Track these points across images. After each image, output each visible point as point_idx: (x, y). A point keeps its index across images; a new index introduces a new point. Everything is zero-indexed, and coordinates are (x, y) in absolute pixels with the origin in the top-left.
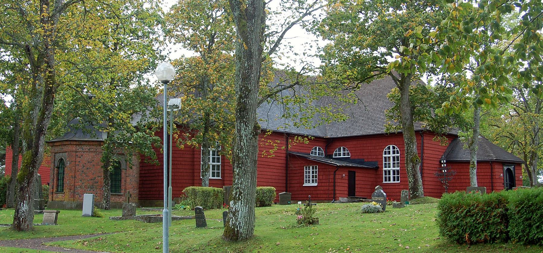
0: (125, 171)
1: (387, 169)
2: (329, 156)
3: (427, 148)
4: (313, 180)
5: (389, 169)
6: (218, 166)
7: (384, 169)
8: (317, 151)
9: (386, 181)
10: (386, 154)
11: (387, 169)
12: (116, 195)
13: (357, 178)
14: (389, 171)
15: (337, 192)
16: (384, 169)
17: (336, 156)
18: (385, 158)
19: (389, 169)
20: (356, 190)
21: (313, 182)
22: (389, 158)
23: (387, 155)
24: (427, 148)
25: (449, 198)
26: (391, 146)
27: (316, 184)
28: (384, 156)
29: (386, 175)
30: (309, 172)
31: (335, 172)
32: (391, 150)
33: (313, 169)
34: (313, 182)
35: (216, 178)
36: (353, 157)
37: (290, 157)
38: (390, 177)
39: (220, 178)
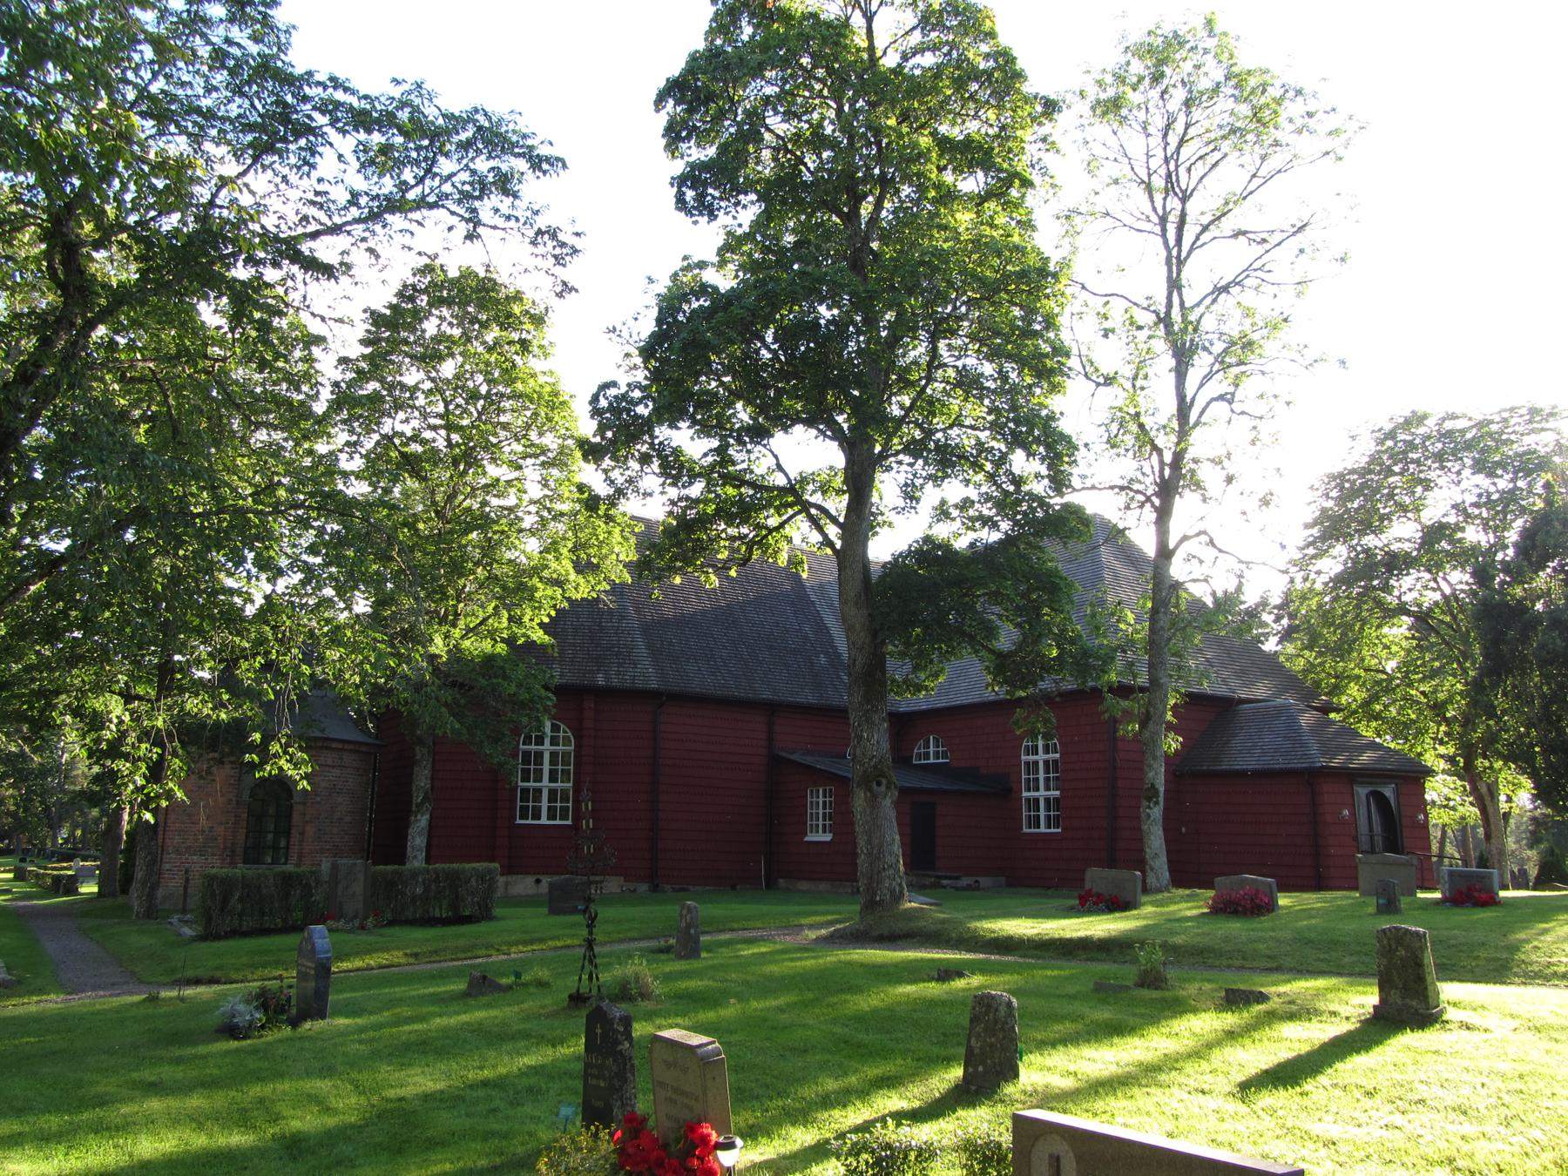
6: (565, 792)
7: (1025, 794)
14: (1037, 800)
16: (1025, 794)
27: (828, 837)
35: (558, 822)
39: (569, 822)
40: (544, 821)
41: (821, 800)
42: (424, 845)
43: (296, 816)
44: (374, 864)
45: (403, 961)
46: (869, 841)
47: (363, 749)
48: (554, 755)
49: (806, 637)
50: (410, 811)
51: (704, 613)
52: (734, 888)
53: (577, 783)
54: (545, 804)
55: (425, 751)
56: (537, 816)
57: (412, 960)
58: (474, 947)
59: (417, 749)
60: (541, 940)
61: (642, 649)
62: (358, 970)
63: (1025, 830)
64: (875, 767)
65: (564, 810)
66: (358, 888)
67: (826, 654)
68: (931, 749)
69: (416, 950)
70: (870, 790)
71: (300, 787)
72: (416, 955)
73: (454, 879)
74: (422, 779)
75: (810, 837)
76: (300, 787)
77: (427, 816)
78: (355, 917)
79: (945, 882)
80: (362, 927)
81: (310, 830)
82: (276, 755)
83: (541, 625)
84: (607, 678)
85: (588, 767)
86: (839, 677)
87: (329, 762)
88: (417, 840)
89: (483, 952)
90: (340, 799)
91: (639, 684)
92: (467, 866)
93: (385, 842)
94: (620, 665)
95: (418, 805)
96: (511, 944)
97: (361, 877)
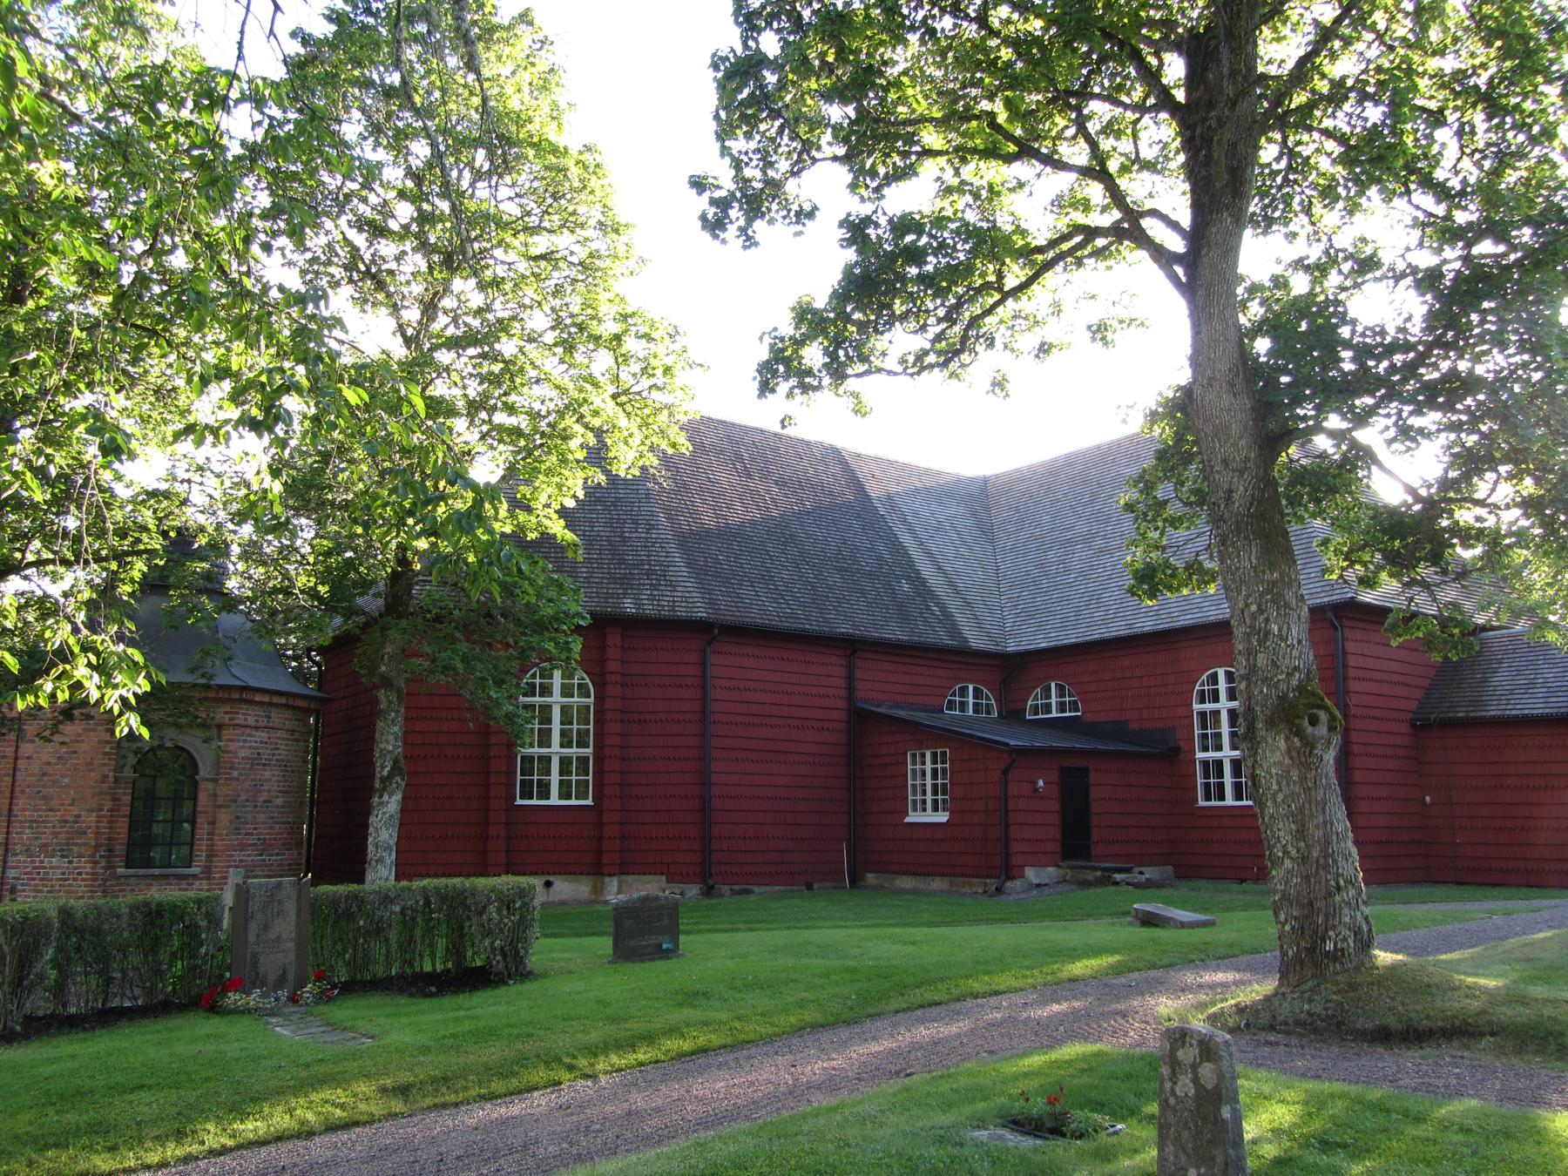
0: (210, 786)
1: (1211, 755)
2: (1012, 714)
3: (1362, 674)
4: (935, 802)
5: (1217, 755)
6: (583, 761)
7: (1200, 755)
8: (971, 700)
9: (1208, 798)
10: (1202, 701)
11: (1211, 755)
12: (166, 877)
13: (1095, 793)
14: (1219, 764)
15: (1015, 847)
16: (1200, 755)
17: (1036, 713)
18: (1203, 715)
19: (1217, 755)
20: (1095, 837)
21: (935, 809)
22: (1217, 713)
23: (1209, 706)
24: (1362, 674)
25: (1472, 521)
26: (1221, 672)
27: (942, 817)
28: (1197, 707)
29: (1207, 776)
30: (924, 773)
31: (1005, 772)
32: (1222, 685)
33: (934, 762)
34: (935, 809)
35: (573, 802)
36: (1090, 717)
37: (861, 721)
38: (1221, 786)
39: (589, 802)
40: (554, 800)
41: (928, 767)
42: (393, 842)
43: (203, 798)
44: (315, 882)
45: (376, 1108)
46: (1301, 834)
47: (299, 703)
48: (565, 710)
49: (881, 558)
50: (370, 790)
51: (753, 523)
52: (809, 887)
53: (599, 747)
54: (555, 778)
55: (393, 697)
56: (545, 794)
57: (398, 1106)
58: (522, 1061)
59: (381, 694)
60: (649, 1038)
61: (680, 568)
62: (280, 1138)
63: (1202, 803)
64: (1301, 688)
65: (583, 785)
66: (286, 927)
67: (908, 578)
68: (1054, 700)
69: (405, 1078)
70: (1299, 733)
71: (121, 731)
72: (403, 1091)
73: (458, 907)
74: (390, 739)
75: (913, 817)
76: (121, 731)
77: (398, 797)
78: (281, 981)
79: (1118, 876)
80: (294, 999)
81: (224, 818)
82: (64, 655)
83: (563, 512)
84: (638, 605)
85: (614, 725)
86: (928, 608)
87: (251, 721)
88: (383, 831)
89: (539, 1075)
90: (267, 774)
91: (681, 612)
92: (482, 882)
93: (335, 849)
94: (653, 587)
95: (383, 780)
96: (594, 1051)
97: (291, 907)
